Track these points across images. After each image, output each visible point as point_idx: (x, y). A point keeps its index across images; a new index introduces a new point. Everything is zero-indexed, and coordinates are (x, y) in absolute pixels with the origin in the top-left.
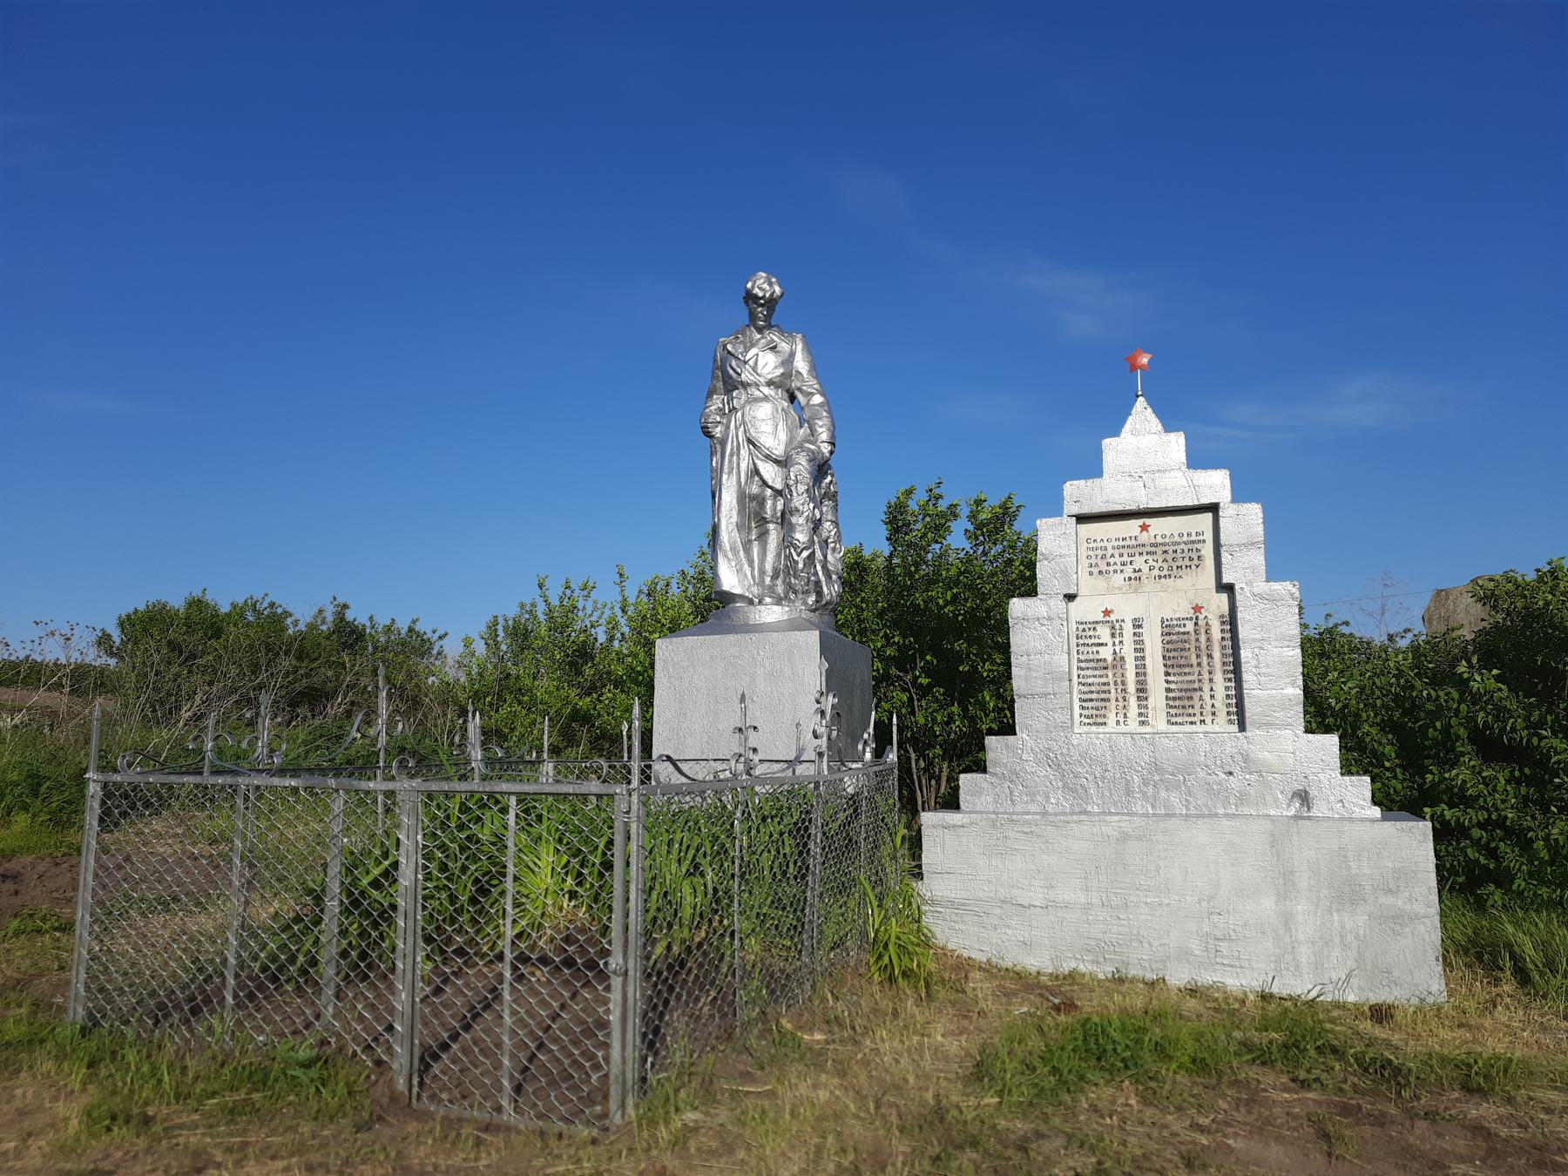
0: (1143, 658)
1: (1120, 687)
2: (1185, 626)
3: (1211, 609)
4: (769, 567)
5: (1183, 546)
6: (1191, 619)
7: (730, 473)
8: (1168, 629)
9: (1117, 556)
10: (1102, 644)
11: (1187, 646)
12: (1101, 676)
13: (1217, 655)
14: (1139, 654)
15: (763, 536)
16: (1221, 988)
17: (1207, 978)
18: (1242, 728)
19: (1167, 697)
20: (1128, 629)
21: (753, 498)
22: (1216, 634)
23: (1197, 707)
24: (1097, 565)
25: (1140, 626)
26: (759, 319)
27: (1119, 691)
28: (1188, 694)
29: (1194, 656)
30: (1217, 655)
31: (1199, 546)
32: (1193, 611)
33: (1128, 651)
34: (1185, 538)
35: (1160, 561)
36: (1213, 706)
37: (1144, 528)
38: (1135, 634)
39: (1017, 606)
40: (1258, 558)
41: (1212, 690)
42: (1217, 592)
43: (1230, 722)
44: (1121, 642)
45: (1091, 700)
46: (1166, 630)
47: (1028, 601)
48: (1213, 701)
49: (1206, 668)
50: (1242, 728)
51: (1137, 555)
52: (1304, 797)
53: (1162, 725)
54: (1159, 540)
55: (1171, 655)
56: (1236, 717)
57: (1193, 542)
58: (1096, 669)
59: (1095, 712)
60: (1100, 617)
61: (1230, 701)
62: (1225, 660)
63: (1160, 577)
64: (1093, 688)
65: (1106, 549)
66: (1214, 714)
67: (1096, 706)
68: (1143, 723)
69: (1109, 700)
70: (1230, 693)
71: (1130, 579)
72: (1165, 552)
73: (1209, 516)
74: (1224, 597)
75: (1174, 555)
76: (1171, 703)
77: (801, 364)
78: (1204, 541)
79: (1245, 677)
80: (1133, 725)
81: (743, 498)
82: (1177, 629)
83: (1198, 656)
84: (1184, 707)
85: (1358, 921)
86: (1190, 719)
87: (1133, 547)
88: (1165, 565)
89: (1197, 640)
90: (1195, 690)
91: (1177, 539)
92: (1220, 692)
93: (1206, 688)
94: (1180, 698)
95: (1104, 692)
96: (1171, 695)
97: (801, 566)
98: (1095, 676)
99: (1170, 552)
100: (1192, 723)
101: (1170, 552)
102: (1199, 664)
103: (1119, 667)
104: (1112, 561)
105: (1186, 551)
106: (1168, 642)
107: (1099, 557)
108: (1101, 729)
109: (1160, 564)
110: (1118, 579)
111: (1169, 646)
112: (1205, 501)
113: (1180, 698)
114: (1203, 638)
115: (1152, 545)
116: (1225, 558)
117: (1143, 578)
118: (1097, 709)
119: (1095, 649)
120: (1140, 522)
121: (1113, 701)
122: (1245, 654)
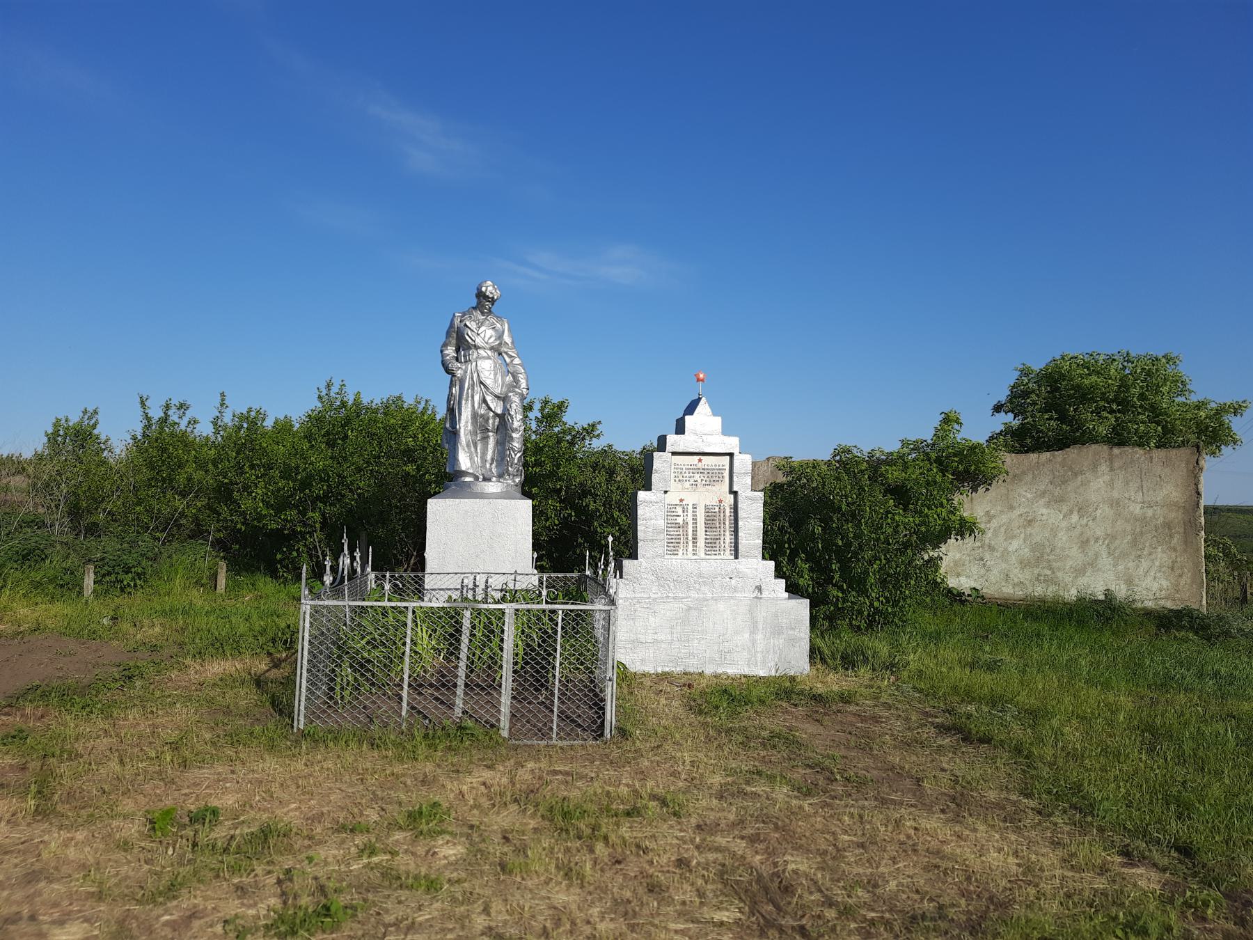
0: (696, 519)
4: (489, 457)
7: (467, 400)
8: (708, 510)
13: (727, 523)
15: (485, 439)
16: (725, 674)
17: (720, 671)
18: (736, 557)
20: (690, 508)
21: (482, 416)
22: (728, 514)
26: (486, 308)
30: (727, 523)
33: (690, 520)
37: (700, 460)
39: (642, 495)
40: (749, 480)
43: (731, 554)
47: (648, 493)
49: (722, 529)
50: (736, 557)
52: (759, 588)
53: (703, 555)
54: (706, 467)
60: (678, 502)
67: (673, 546)
68: (694, 554)
69: (679, 543)
73: (728, 457)
74: (732, 496)
77: (507, 338)
79: (740, 534)
80: (690, 555)
81: (475, 415)
85: (780, 642)
92: (728, 541)
93: (722, 539)
97: (516, 461)
108: (676, 557)
110: (687, 485)
112: (728, 451)
114: (722, 515)
115: (703, 469)
116: (735, 479)
120: (698, 457)
122: (740, 523)
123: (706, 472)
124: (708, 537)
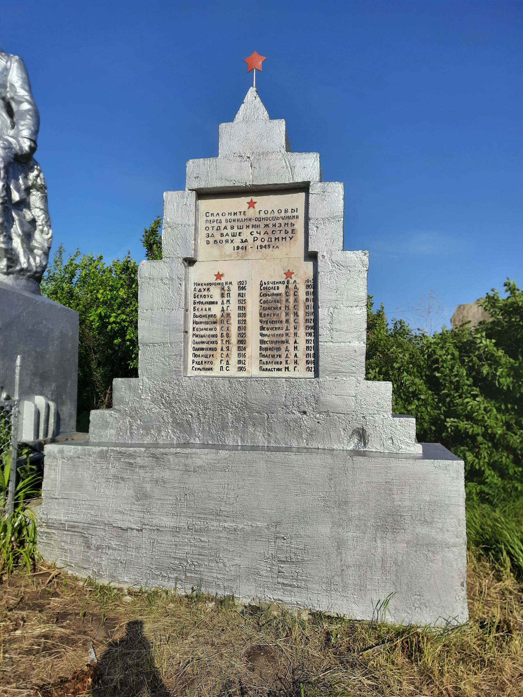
0: (245, 315)
1: (225, 338)
2: (278, 288)
3: (299, 275)
5: (280, 221)
6: (283, 283)
10: (213, 303)
11: (279, 305)
12: (211, 329)
14: (241, 312)
24: (213, 235)
25: (244, 288)
28: (277, 346)
29: (284, 314)
32: (285, 276)
34: (283, 214)
35: (262, 233)
36: (296, 356)
41: (295, 342)
42: (305, 260)
44: (228, 301)
45: (202, 349)
48: (296, 352)
51: (245, 227)
55: (266, 312)
57: (289, 218)
59: (204, 359)
61: (309, 352)
62: (307, 318)
63: (261, 247)
64: (204, 339)
66: (296, 362)
69: (216, 336)
70: (309, 345)
71: (238, 248)
72: (267, 226)
75: (274, 229)
76: (264, 353)
78: (297, 217)
82: (272, 291)
83: (287, 314)
84: (273, 356)
86: (277, 366)
88: (266, 239)
89: (287, 300)
90: (283, 342)
91: (276, 214)
94: (270, 349)
95: (213, 342)
96: (264, 346)
98: (206, 329)
99: (271, 226)
100: (279, 370)
101: (271, 226)
102: (287, 321)
103: (225, 322)
104: (225, 232)
105: (283, 225)
106: (265, 302)
107: (215, 228)
109: (262, 235)
110: (229, 248)
111: (265, 305)
113: (270, 349)
117: (249, 247)
119: (207, 306)
121: (219, 350)
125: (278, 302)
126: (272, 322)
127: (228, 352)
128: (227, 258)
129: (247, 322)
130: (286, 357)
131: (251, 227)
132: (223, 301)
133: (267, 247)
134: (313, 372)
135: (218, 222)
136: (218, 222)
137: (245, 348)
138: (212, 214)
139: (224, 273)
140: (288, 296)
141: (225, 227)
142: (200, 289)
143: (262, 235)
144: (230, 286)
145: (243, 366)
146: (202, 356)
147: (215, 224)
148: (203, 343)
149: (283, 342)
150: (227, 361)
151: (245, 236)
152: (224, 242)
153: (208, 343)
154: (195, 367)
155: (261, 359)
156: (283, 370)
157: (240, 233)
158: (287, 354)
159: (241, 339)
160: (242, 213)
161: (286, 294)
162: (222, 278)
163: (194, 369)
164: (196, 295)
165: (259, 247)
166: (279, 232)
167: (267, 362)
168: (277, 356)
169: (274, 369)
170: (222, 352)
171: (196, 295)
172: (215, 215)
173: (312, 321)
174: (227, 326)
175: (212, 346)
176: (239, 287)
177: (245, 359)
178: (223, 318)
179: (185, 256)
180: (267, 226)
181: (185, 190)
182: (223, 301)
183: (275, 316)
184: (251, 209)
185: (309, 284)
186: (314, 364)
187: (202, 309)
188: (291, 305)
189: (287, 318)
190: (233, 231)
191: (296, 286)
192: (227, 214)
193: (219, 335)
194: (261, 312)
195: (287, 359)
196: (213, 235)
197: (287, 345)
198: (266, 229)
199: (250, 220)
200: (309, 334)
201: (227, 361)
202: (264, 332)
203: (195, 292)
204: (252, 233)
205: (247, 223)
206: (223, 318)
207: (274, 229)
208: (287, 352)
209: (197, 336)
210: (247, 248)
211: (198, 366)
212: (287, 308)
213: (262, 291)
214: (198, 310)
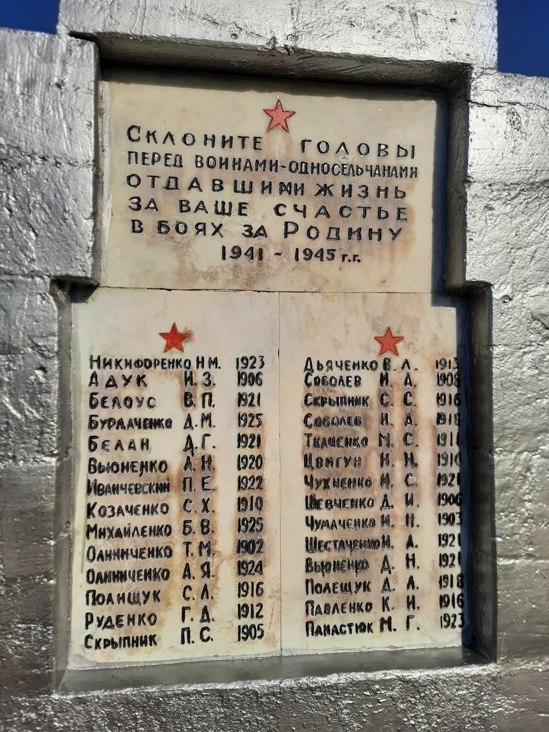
0: (258, 461)
1: (198, 538)
2: (358, 382)
3: (418, 345)
5: (365, 179)
6: (373, 365)
9: (206, 185)
10: (155, 424)
11: (361, 433)
12: (148, 510)
14: (248, 452)
19: (308, 562)
23: (376, 585)
24: (153, 205)
25: (255, 379)
27: (194, 548)
28: (357, 555)
29: (375, 459)
31: (402, 183)
32: (377, 347)
34: (372, 160)
35: (311, 211)
36: (411, 583)
38: (240, 397)
41: (410, 543)
42: (436, 302)
44: (206, 418)
45: (121, 576)
46: (316, 391)
48: (412, 571)
51: (257, 188)
55: (325, 453)
56: (458, 610)
57: (388, 171)
58: (137, 489)
59: (126, 609)
61: (447, 571)
62: (442, 470)
63: (309, 254)
64: (126, 543)
65: (179, 163)
66: (411, 603)
69: (167, 530)
70: (448, 550)
71: (237, 252)
72: (325, 189)
75: (345, 202)
76: (318, 578)
78: (414, 172)
82: (341, 391)
83: (384, 460)
84: (346, 588)
86: (357, 618)
87: (248, 166)
88: (323, 228)
89: (384, 419)
90: (373, 544)
91: (353, 158)
94: (338, 566)
95: (155, 553)
96: (318, 557)
98: (133, 510)
99: (337, 191)
100: (363, 628)
101: (337, 191)
102: (385, 480)
103: (197, 485)
104: (194, 197)
105: (372, 192)
106: (319, 422)
107: (161, 183)
109: (310, 220)
111: (321, 433)
113: (338, 566)
117: (269, 254)
118: (133, 599)
119: (138, 435)
121: (177, 578)
123: (311, 189)
124: (324, 535)
125: (357, 422)
126: (340, 483)
127: (207, 581)
128: (201, 283)
129: (268, 483)
130: (384, 589)
131: (276, 188)
132: (189, 419)
133: (325, 255)
134: (459, 630)
135: (171, 162)
136: (171, 162)
137: (260, 564)
138: (150, 135)
139: (190, 328)
140: (386, 405)
141: (195, 180)
142: (112, 379)
143: (310, 220)
144: (213, 370)
145: (256, 622)
146: (121, 598)
147: (159, 168)
148: (123, 554)
149: (373, 544)
150: (205, 611)
151: (259, 217)
152: (192, 230)
153: (139, 554)
154: (96, 637)
155: (311, 597)
156: (376, 627)
157: (242, 206)
158: (387, 581)
159: (247, 537)
160: (249, 143)
161: (382, 399)
162: (186, 346)
163: (92, 642)
164: (99, 397)
165: (301, 256)
166: (361, 212)
167: (327, 606)
168: (358, 586)
169: (350, 625)
170: (187, 582)
171: (99, 397)
172: (160, 136)
173: (455, 482)
174: (204, 495)
175: (153, 563)
176: (240, 376)
177: (261, 600)
178: (189, 473)
179: (60, 270)
180: (325, 189)
181: (52, 31)
182: (189, 419)
183: (351, 466)
184: (278, 136)
185: (447, 371)
186: (462, 606)
187: (119, 445)
188: (397, 435)
189: (386, 470)
190: (220, 197)
191: (408, 376)
192: (200, 139)
193: (177, 527)
194: (307, 452)
195: (386, 594)
196: (153, 205)
197: (387, 551)
198: (322, 200)
199: (274, 166)
200: (448, 519)
201: (205, 611)
202: (320, 515)
203: (93, 389)
204: (281, 210)
205: (266, 176)
206: (189, 473)
207: (345, 202)
208: (386, 573)
209: (102, 534)
210: (265, 255)
211: (107, 634)
212: (384, 442)
213: (313, 390)
214: (104, 445)
